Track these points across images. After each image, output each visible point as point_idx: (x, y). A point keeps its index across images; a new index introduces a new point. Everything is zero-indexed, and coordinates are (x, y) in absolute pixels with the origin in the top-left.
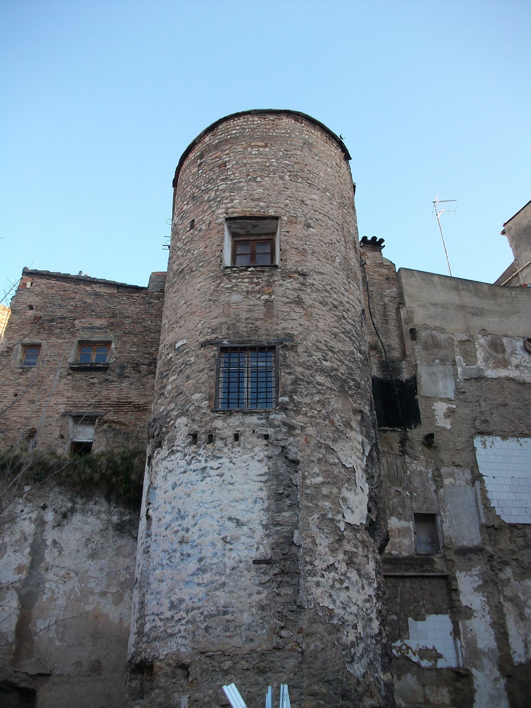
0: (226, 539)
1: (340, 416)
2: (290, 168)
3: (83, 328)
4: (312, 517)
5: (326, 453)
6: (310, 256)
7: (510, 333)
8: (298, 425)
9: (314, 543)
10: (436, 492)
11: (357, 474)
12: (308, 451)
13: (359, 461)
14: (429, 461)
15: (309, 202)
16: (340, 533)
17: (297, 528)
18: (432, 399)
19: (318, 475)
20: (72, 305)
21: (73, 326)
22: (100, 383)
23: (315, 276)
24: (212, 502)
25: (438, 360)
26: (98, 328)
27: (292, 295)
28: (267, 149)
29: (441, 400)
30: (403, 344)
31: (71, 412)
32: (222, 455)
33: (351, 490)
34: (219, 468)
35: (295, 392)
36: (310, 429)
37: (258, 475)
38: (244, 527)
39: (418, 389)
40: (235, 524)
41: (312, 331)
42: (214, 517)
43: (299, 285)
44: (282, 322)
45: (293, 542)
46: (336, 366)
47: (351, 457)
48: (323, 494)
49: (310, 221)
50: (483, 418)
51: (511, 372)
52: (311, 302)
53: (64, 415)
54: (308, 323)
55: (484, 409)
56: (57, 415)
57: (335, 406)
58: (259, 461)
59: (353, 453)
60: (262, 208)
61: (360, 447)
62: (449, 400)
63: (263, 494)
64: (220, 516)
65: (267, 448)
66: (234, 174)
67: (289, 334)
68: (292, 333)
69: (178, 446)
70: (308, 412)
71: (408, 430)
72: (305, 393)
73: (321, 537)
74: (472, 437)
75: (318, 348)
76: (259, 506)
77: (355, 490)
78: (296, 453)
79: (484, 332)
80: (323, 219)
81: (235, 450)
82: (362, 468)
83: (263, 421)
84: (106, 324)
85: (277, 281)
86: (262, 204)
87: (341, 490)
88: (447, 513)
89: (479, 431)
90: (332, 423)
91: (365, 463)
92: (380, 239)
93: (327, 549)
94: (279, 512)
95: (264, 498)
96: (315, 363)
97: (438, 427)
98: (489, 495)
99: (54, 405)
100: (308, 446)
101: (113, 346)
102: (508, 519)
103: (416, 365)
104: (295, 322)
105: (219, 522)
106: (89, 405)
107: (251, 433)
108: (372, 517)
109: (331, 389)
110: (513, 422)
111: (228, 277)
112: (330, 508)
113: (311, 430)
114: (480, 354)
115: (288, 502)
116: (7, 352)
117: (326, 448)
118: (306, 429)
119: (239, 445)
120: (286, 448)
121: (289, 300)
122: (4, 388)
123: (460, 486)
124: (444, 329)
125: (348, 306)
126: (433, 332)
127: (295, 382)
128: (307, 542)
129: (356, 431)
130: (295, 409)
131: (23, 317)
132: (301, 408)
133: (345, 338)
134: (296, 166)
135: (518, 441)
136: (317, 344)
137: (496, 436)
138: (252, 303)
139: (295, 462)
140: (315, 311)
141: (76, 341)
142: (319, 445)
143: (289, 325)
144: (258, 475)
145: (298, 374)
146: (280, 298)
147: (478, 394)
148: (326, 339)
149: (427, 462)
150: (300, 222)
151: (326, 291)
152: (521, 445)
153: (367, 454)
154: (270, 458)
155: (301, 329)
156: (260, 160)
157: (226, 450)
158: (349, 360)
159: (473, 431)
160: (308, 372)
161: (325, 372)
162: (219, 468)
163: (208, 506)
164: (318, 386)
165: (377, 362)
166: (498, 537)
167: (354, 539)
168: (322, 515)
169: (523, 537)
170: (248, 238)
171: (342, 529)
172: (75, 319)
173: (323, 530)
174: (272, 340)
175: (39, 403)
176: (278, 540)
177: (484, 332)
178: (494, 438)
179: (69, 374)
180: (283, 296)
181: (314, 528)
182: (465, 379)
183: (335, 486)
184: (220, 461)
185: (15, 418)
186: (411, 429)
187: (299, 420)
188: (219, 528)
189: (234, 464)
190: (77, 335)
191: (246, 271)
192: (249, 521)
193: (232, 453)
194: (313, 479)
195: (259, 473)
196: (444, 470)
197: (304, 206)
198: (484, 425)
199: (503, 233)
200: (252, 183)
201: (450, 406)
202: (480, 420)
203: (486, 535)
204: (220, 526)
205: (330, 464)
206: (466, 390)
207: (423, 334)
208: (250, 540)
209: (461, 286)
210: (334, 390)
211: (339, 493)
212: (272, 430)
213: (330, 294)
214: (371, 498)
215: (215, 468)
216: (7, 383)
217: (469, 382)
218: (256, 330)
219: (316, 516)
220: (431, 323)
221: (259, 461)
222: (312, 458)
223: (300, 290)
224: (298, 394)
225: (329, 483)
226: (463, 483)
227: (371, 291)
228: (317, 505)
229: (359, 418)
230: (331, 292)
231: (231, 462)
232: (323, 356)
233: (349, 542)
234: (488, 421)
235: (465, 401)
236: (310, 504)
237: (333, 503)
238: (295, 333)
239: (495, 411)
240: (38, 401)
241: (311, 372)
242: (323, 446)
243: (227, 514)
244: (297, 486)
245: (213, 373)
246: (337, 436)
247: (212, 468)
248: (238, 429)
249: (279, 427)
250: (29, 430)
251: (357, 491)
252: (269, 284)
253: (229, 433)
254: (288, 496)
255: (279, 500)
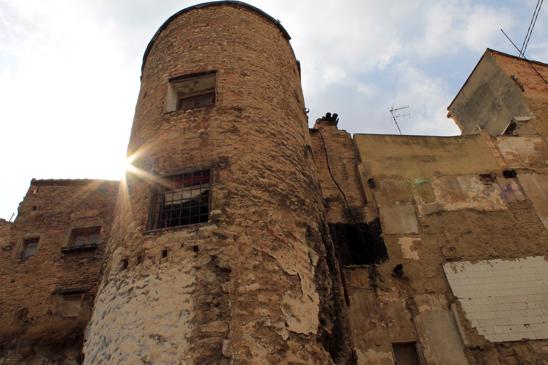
0: (146, 359)
1: (280, 226)
2: (227, 37)
3: (77, 218)
4: (247, 326)
5: (264, 260)
6: (246, 96)
7: (462, 172)
8: (231, 235)
9: (249, 354)
10: (412, 320)
11: (302, 282)
12: (242, 259)
13: (306, 271)
14: (402, 291)
15: (245, 58)
16: (282, 343)
17: (227, 338)
18: (396, 236)
19: (253, 282)
20: (69, 202)
21: (69, 218)
22: (88, 262)
23: (251, 110)
24: (135, 321)
25: (398, 202)
26: (90, 217)
27: (227, 126)
28: (209, 27)
29: (406, 235)
30: (363, 194)
31: (61, 290)
32: (149, 273)
33: (295, 297)
34: (145, 286)
35: (228, 204)
36: (245, 237)
37: (188, 286)
38: (166, 343)
39: (382, 228)
40: (156, 341)
41: (247, 153)
42: (135, 337)
43: (235, 118)
44: (217, 148)
45: (222, 355)
46: (275, 183)
47: (295, 265)
48: (259, 302)
49: (246, 72)
50: (449, 246)
51: (470, 204)
52: (246, 130)
53: (54, 293)
54: (243, 147)
55: (449, 238)
56: (48, 294)
57: (274, 217)
58: (186, 273)
59: (297, 261)
60: (201, 66)
61: (306, 257)
62: (414, 234)
63: (190, 306)
64: (141, 334)
65: (196, 259)
66: (179, 48)
67: (224, 157)
68: (226, 156)
69: (112, 275)
70: (242, 223)
71: (376, 265)
72: (240, 205)
73: (257, 347)
74: (441, 265)
75: (253, 167)
76: (184, 319)
77: (300, 298)
78: (228, 261)
79: (438, 174)
80: (260, 70)
81: (162, 265)
82: (309, 277)
83: (193, 234)
84: (98, 213)
85: (212, 116)
86: (201, 64)
87: (282, 297)
88: (427, 339)
89: (447, 258)
90: (272, 232)
91: (314, 273)
92: (334, 115)
93: (265, 360)
94: (206, 321)
95: (190, 309)
96: (251, 179)
97: (406, 259)
98: (468, 317)
99: (47, 286)
100: (242, 254)
101: (102, 230)
102: (493, 339)
103: (378, 209)
104: (229, 146)
105: (140, 342)
106: (78, 282)
107: (180, 247)
108: (326, 329)
109: (270, 202)
110: (481, 247)
111: (168, 120)
112: (269, 316)
113: (244, 239)
114: (438, 192)
115: (217, 311)
116: (10, 246)
117: (263, 255)
118: (240, 238)
119: (167, 260)
120: (216, 257)
121: (224, 130)
122: (4, 277)
123: (437, 312)
124: (400, 177)
125: (287, 135)
126: (390, 179)
127: (229, 195)
128: (240, 353)
129: (301, 242)
130: (227, 220)
131: (27, 217)
132: (234, 219)
133: (284, 160)
134: (234, 36)
135: (488, 263)
136: (253, 163)
137: (465, 260)
138: (188, 137)
139: (227, 270)
140: (250, 138)
141: (70, 230)
142: (255, 253)
143: (223, 150)
144: (184, 287)
145: (231, 189)
146: (215, 130)
147: (441, 226)
148: (263, 160)
149: (399, 293)
150: (237, 72)
151: (263, 122)
152: (492, 266)
153: (315, 264)
154: (198, 268)
155: (236, 152)
156: (201, 35)
157: (153, 267)
158: (290, 179)
159: (441, 259)
160: (242, 187)
161: (262, 188)
162: (145, 286)
163: (129, 327)
164: (254, 199)
165: (341, 211)
166: (486, 358)
167: (302, 350)
168: (258, 323)
169: (513, 355)
170: (192, 95)
171: (285, 338)
172: (71, 213)
173: (260, 339)
174: (207, 164)
175: (32, 286)
176: (204, 353)
177: (438, 174)
178: (464, 262)
179: (62, 258)
180: (218, 127)
181: (248, 337)
182: (426, 215)
183: (275, 293)
184: (147, 279)
185: (9, 302)
186: (379, 264)
187: (232, 230)
188: (139, 348)
189: (160, 279)
190: (72, 224)
191: (185, 113)
192: (172, 336)
193: (159, 269)
194: (247, 287)
195: (185, 285)
196: (417, 298)
197: (241, 61)
198: (451, 252)
199: (449, 116)
200: (193, 51)
201: (415, 239)
202: (447, 248)
203: (472, 357)
204: (141, 346)
205: (269, 272)
206: (429, 224)
207: (382, 183)
208: (172, 356)
209: (411, 141)
210: (273, 203)
211: (279, 300)
212: (202, 241)
213: (267, 124)
214: (323, 310)
215: (141, 286)
216: (6, 272)
217: (431, 217)
218: (191, 159)
219: (251, 324)
220: (387, 173)
221: (186, 273)
222: (246, 266)
223: (235, 121)
224: (231, 206)
225: (267, 290)
226: (440, 309)
227: (330, 156)
228: (252, 313)
229: (304, 230)
230: (269, 123)
231: (157, 278)
232: (259, 173)
233: (294, 352)
234: (454, 248)
235: (429, 234)
236: (244, 312)
237: (272, 310)
238: (230, 155)
239: (460, 239)
240: (32, 284)
241: (246, 187)
242: (260, 254)
243: (149, 331)
244: (227, 293)
245: (147, 200)
246: (276, 245)
247: (138, 288)
248: (166, 245)
249: (209, 237)
250: (21, 311)
251: (304, 299)
252: (205, 120)
253: (158, 251)
254: (217, 305)
255: (207, 310)
